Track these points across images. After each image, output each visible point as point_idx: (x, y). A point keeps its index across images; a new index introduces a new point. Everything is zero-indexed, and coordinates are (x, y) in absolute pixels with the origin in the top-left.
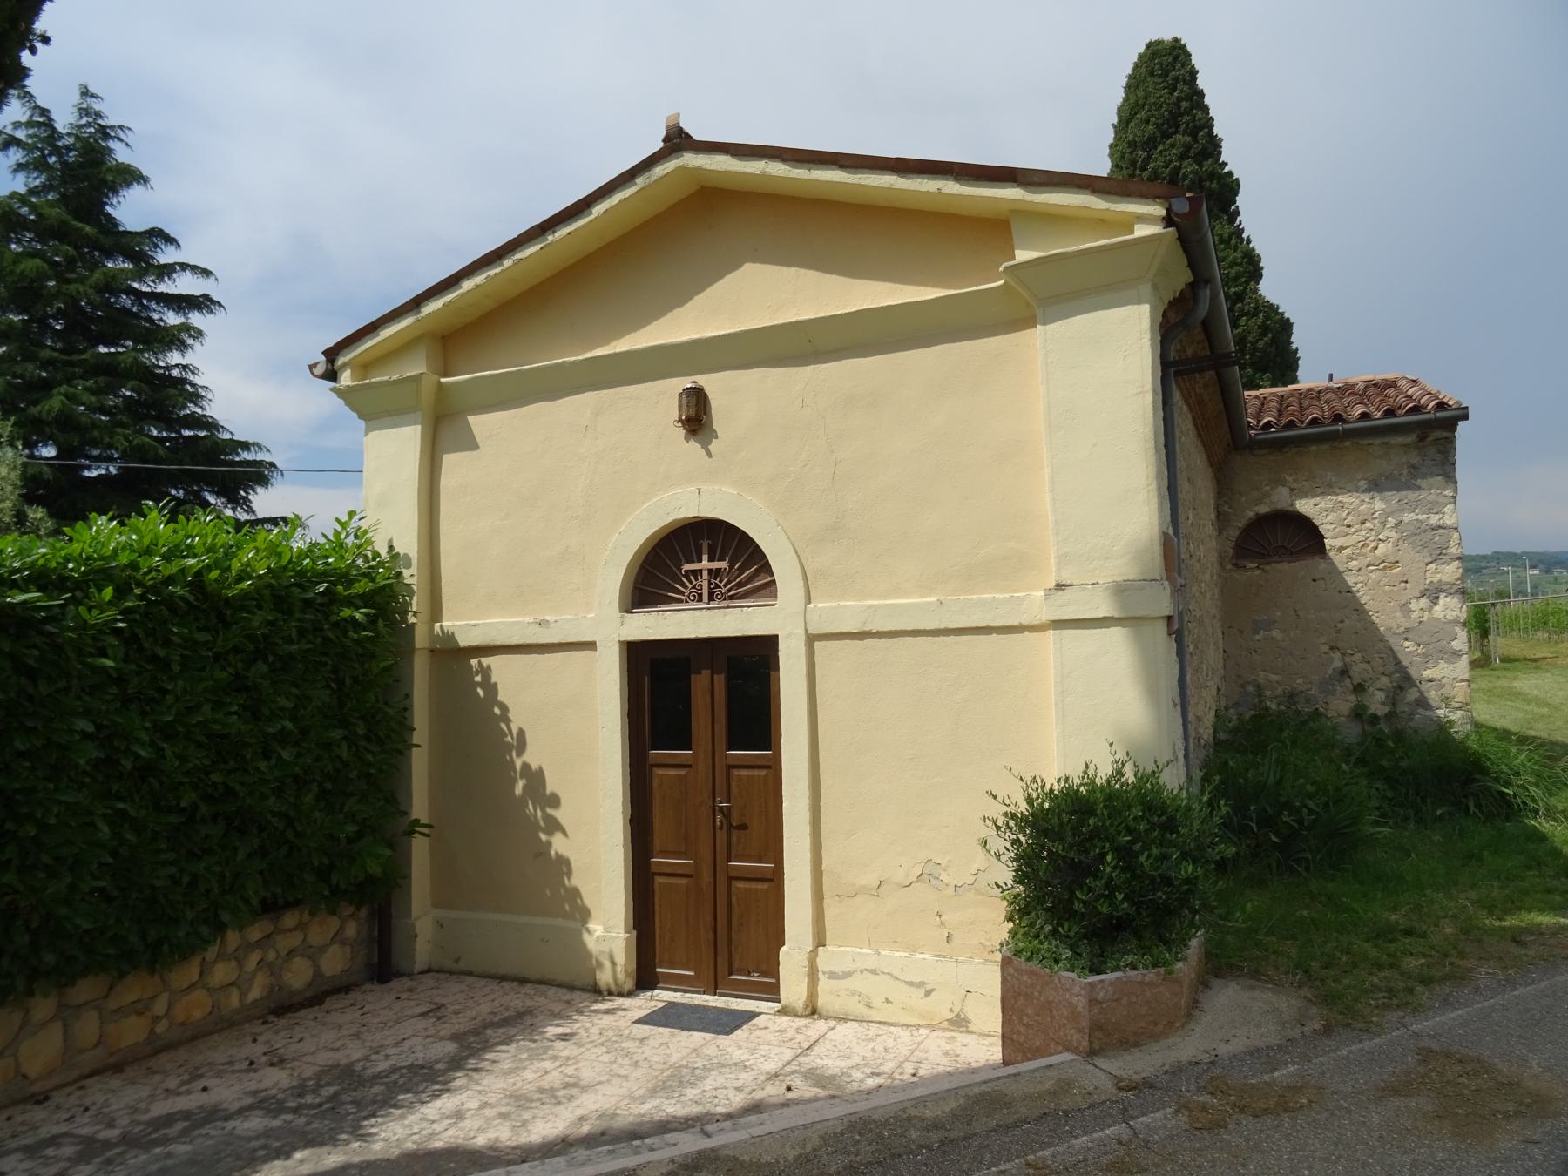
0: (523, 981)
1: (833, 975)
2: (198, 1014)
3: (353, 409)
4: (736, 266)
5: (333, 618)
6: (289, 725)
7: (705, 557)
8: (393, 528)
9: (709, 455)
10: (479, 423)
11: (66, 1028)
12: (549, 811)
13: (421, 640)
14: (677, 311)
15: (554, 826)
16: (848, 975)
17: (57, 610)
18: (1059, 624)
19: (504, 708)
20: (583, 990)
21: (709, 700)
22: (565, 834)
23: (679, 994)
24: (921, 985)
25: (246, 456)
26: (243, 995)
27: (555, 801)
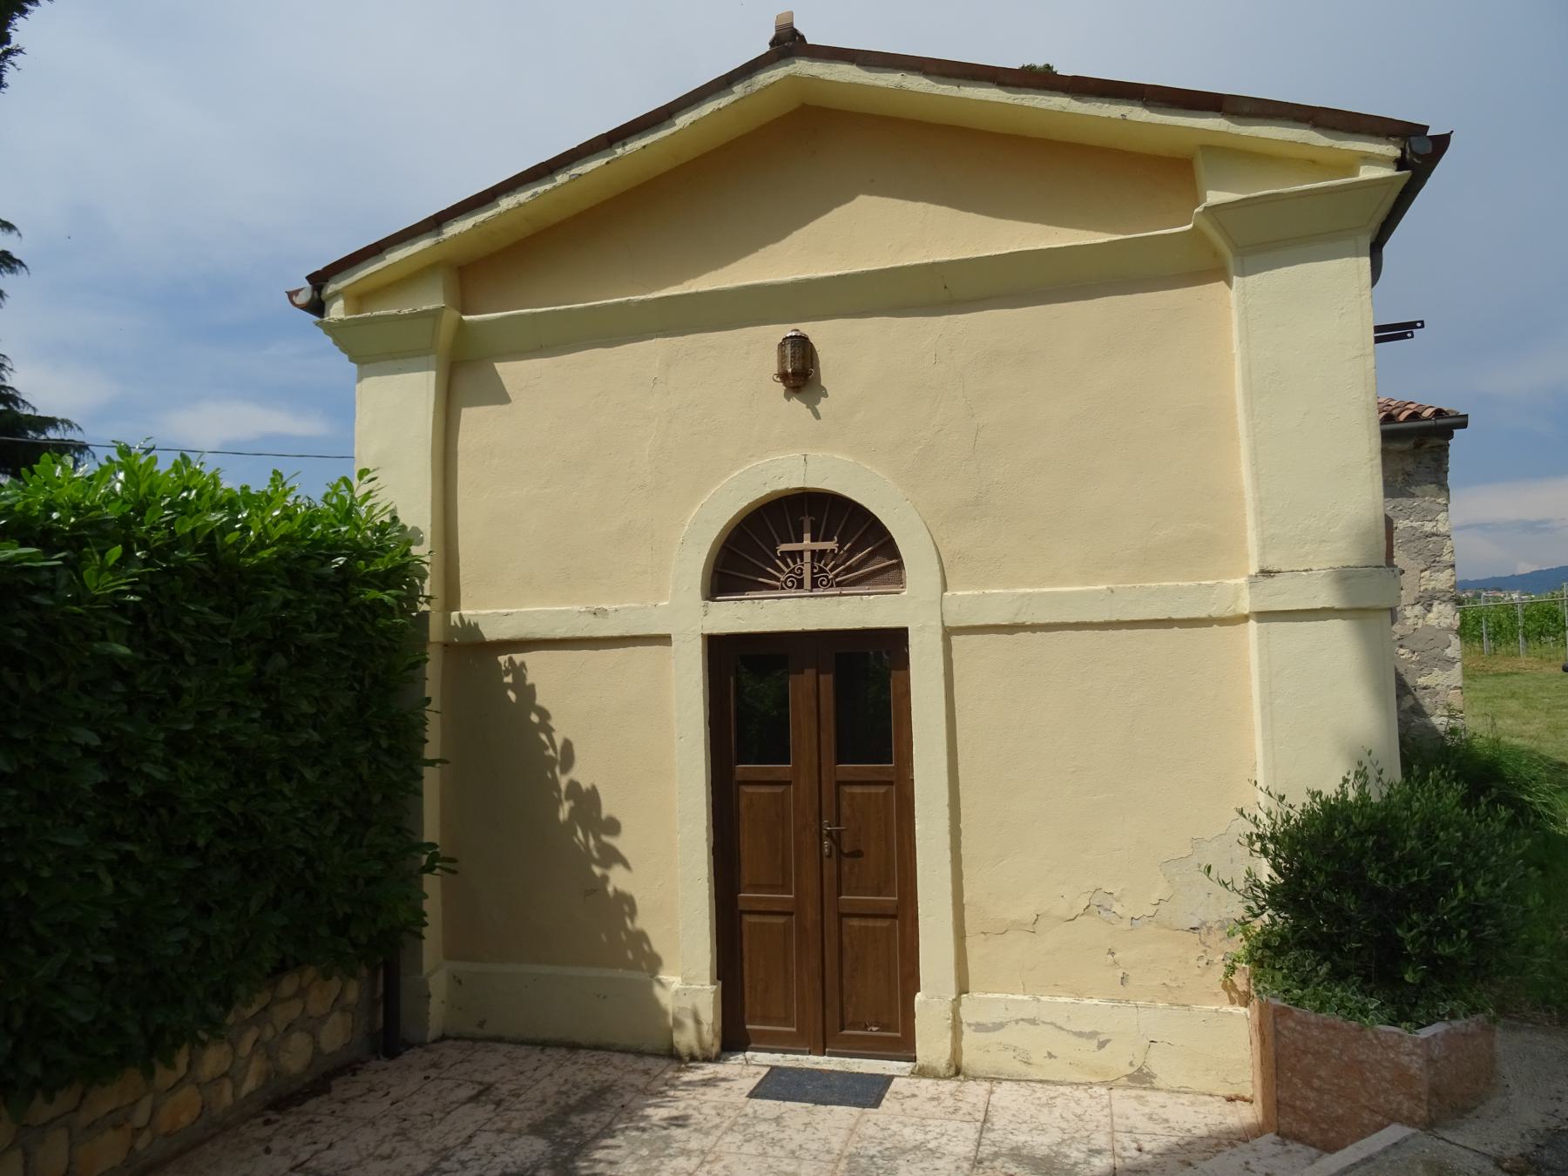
0: (574, 1047)
1: (980, 1027)
2: (185, 1119)
3: (344, 349)
4: (850, 198)
5: (354, 601)
6: (316, 737)
7: (807, 536)
8: (402, 495)
9: (817, 416)
10: (507, 371)
11: (27, 1155)
12: (605, 838)
13: (435, 632)
15: (612, 857)
16: (999, 1026)
17: (47, 575)
18: (1264, 616)
19: (544, 714)
20: (656, 1055)
21: (813, 703)
23: (778, 1056)
24: (1093, 1035)
25: (52, 434)
26: (236, 1086)
27: (613, 827)
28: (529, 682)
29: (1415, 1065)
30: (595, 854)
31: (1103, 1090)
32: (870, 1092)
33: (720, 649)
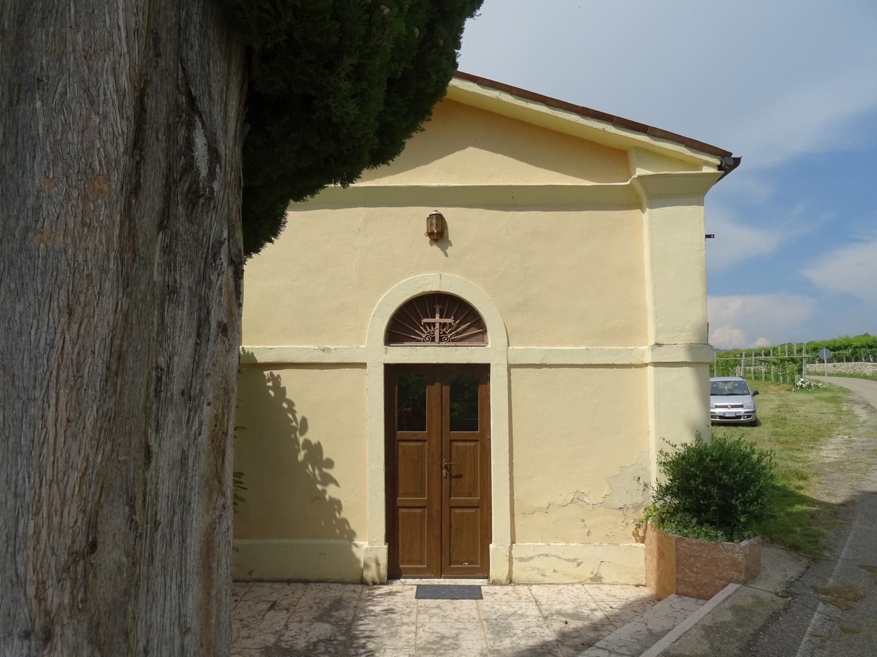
1: (521, 560)
4: (464, 147)
7: (438, 316)
9: (446, 255)
12: (325, 470)
14: (422, 167)
15: (328, 480)
16: (531, 558)
18: (656, 364)
19: (291, 404)
21: (439, 401)
22: (337, 484)
24: (575, 560)
27: (330, 464)
28: (282, 386)
29: (740, 558)
30: (319, 479)
31: (580, 586)
32: (475, 593)
33: (393, 372)
